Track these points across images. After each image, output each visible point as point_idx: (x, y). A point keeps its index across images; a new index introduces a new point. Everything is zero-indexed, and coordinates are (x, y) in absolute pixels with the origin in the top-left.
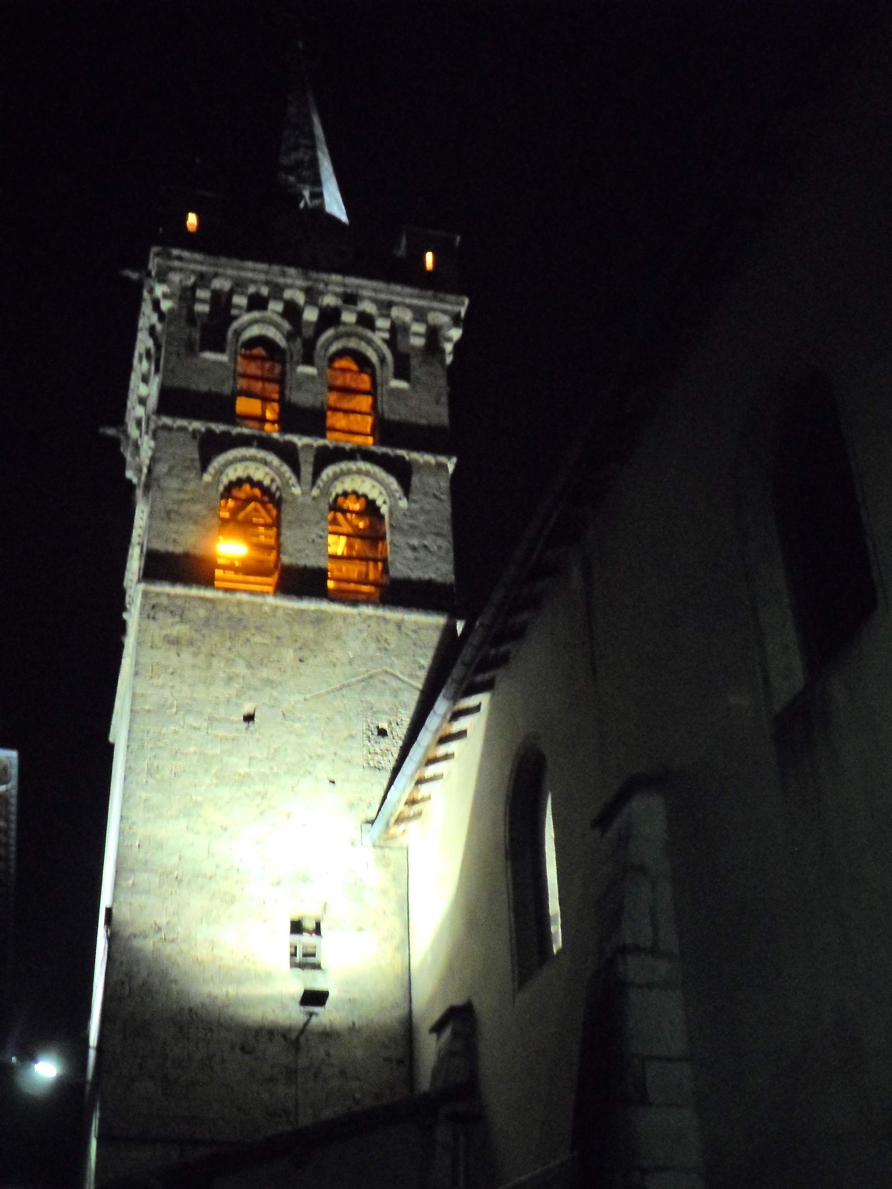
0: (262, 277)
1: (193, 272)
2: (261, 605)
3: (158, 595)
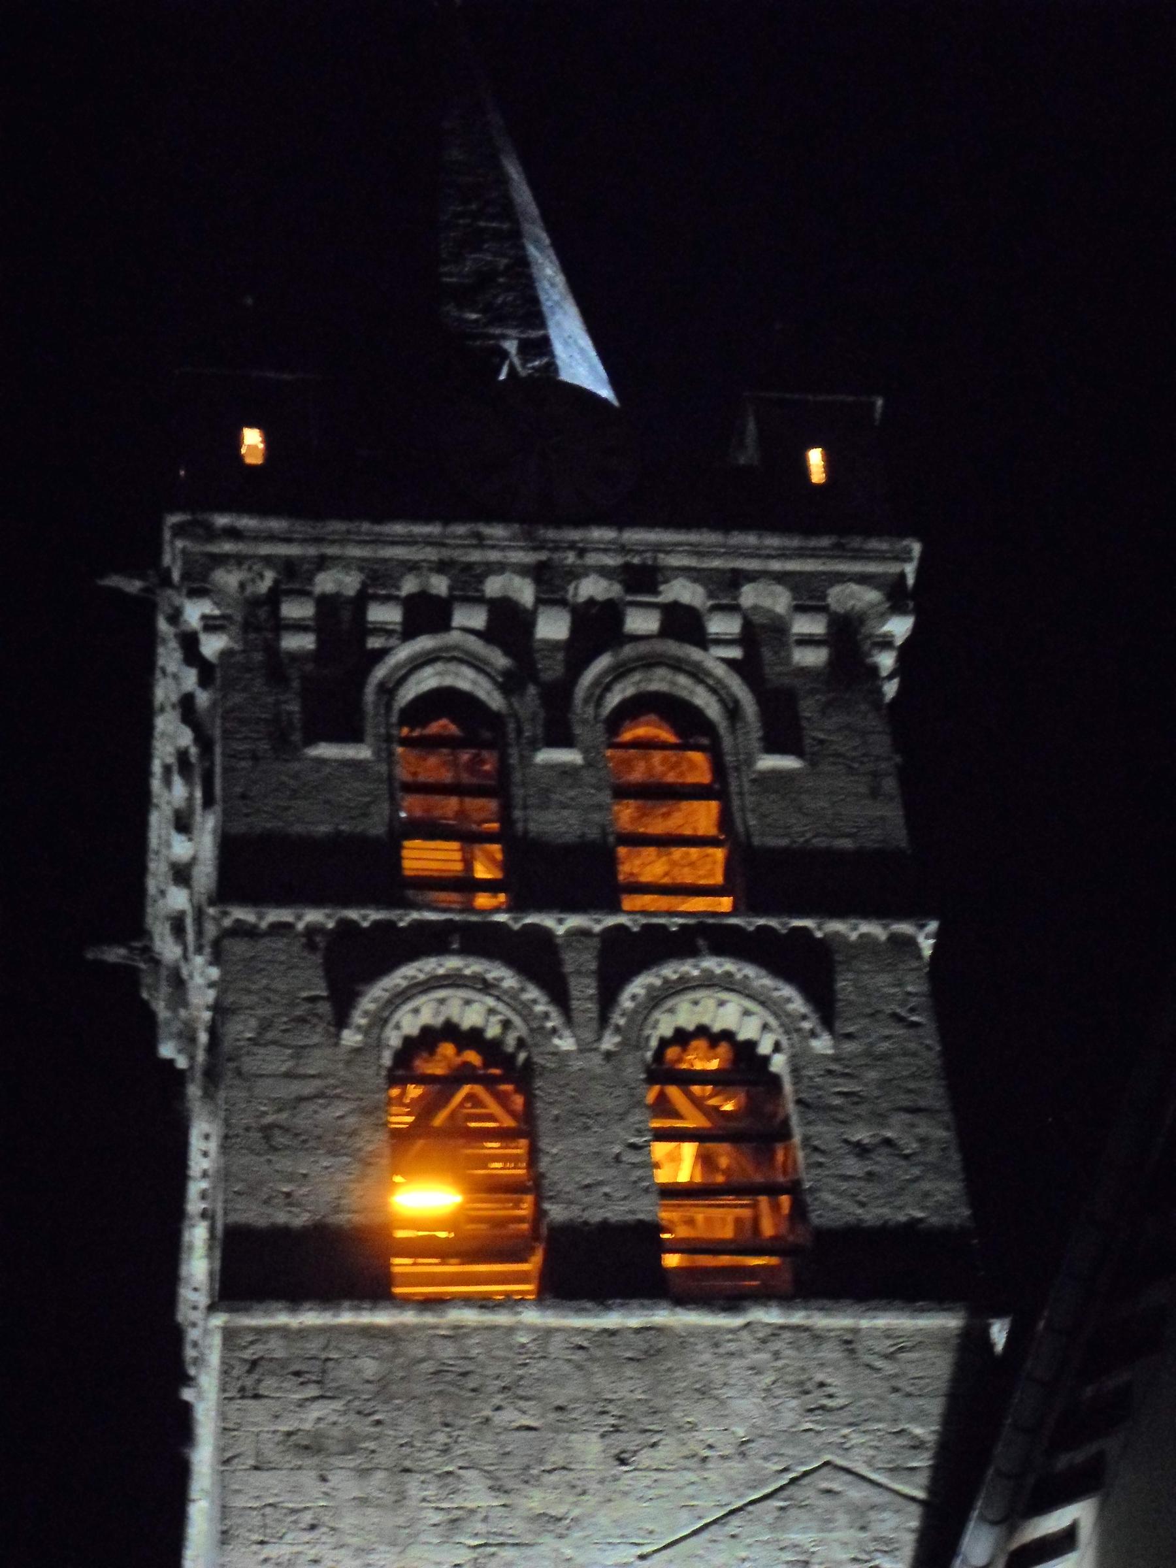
0: (431, 554)
3: (261, 1333)
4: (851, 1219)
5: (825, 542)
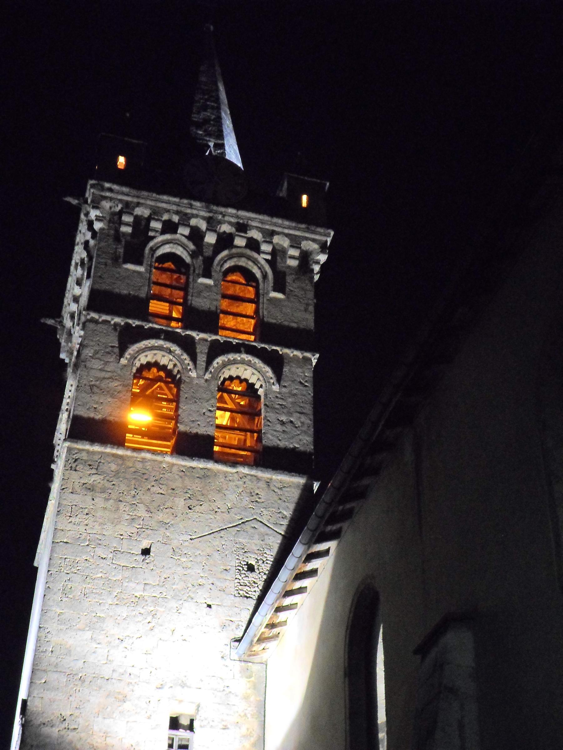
0: (174, 208)
1: (121, 201)
2: (161, 462)
4: (276, 444)
5: (303, 226)
